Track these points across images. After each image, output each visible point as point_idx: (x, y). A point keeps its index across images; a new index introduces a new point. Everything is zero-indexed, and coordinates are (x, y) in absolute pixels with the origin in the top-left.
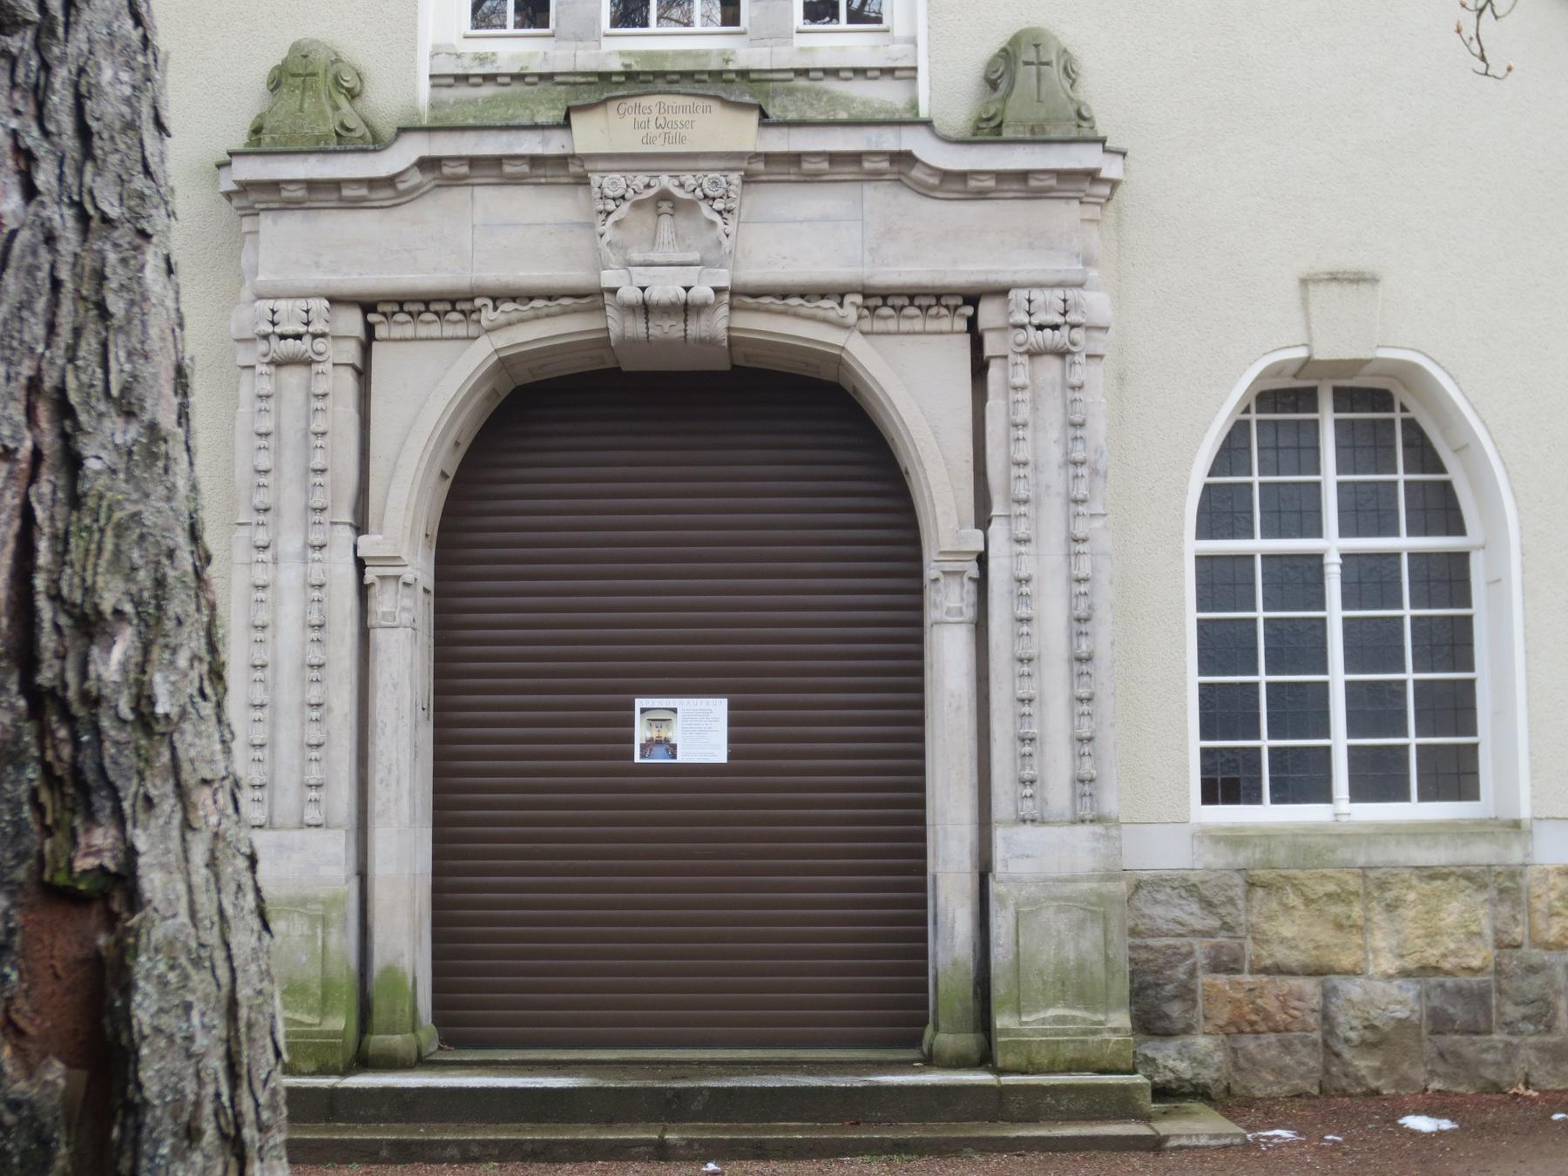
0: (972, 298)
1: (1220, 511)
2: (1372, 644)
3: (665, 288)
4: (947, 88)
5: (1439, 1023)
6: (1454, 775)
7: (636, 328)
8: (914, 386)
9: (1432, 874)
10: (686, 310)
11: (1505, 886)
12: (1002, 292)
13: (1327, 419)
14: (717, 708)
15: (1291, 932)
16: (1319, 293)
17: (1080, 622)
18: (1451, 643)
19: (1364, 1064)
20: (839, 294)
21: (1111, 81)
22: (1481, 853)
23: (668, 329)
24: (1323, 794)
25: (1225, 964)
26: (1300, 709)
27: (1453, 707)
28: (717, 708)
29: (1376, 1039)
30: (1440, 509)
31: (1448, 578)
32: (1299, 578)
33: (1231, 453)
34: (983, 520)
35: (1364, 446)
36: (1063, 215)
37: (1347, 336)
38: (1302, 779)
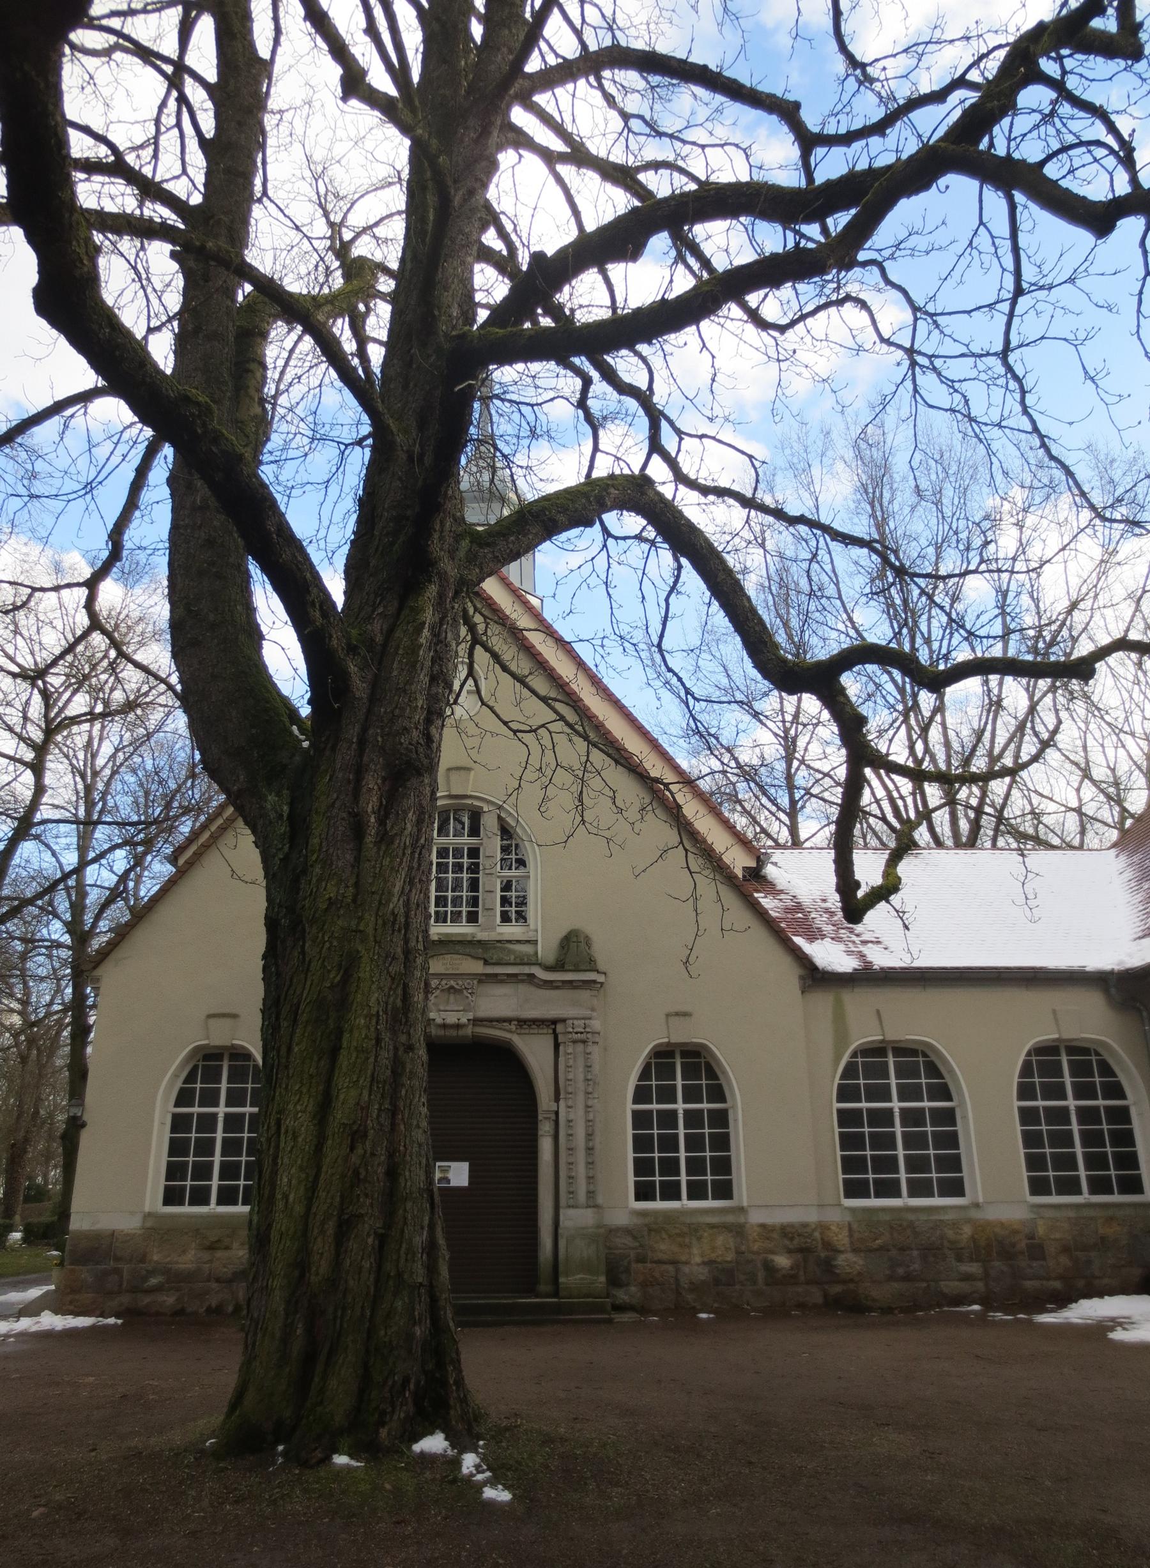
0: (555, 1022)
1: (1025, 1092)
2: (694, 1143)
3: (452, 1019)
4: (546, 949)
5: (717, 1281)
6: (724, 1190)
7: (441, 1032)
8: (536, 1052)
9: (712, 1226)
10: (458, 1026)
11: (738, 1230)
12: (564, 1020)
13: (891, 1060)
14: (465, 1166)
15: (664, 1247)
16: (212, 1021)
17: (589, 1136)
18: (722, 1142)
19: (690, 1297)
20: (509, 1020)
21: (601, 951)
22: (730, 1219)
23: (453, 1033)
24: (206, 1202)
25: (641, 1259)
26: (203, 1172)
27: (723, 1166)
28: (465, 1166)
29: (695, 1287)
30: (717, 1094)
31: (721, 1119)
32: (208, 1123)
33: (645, 1074)
34: (557, 1099)
35: (1080, 1069)
36: (585, 995)
37: (682, 1034)
38: (670, 1191)
